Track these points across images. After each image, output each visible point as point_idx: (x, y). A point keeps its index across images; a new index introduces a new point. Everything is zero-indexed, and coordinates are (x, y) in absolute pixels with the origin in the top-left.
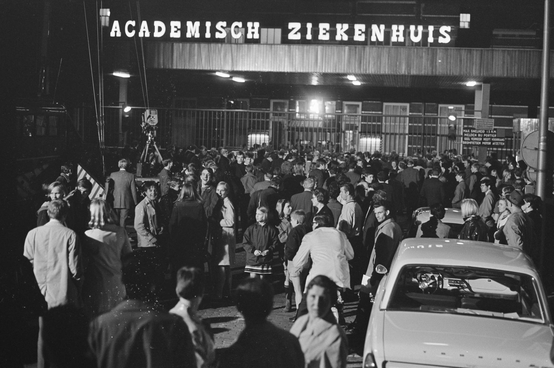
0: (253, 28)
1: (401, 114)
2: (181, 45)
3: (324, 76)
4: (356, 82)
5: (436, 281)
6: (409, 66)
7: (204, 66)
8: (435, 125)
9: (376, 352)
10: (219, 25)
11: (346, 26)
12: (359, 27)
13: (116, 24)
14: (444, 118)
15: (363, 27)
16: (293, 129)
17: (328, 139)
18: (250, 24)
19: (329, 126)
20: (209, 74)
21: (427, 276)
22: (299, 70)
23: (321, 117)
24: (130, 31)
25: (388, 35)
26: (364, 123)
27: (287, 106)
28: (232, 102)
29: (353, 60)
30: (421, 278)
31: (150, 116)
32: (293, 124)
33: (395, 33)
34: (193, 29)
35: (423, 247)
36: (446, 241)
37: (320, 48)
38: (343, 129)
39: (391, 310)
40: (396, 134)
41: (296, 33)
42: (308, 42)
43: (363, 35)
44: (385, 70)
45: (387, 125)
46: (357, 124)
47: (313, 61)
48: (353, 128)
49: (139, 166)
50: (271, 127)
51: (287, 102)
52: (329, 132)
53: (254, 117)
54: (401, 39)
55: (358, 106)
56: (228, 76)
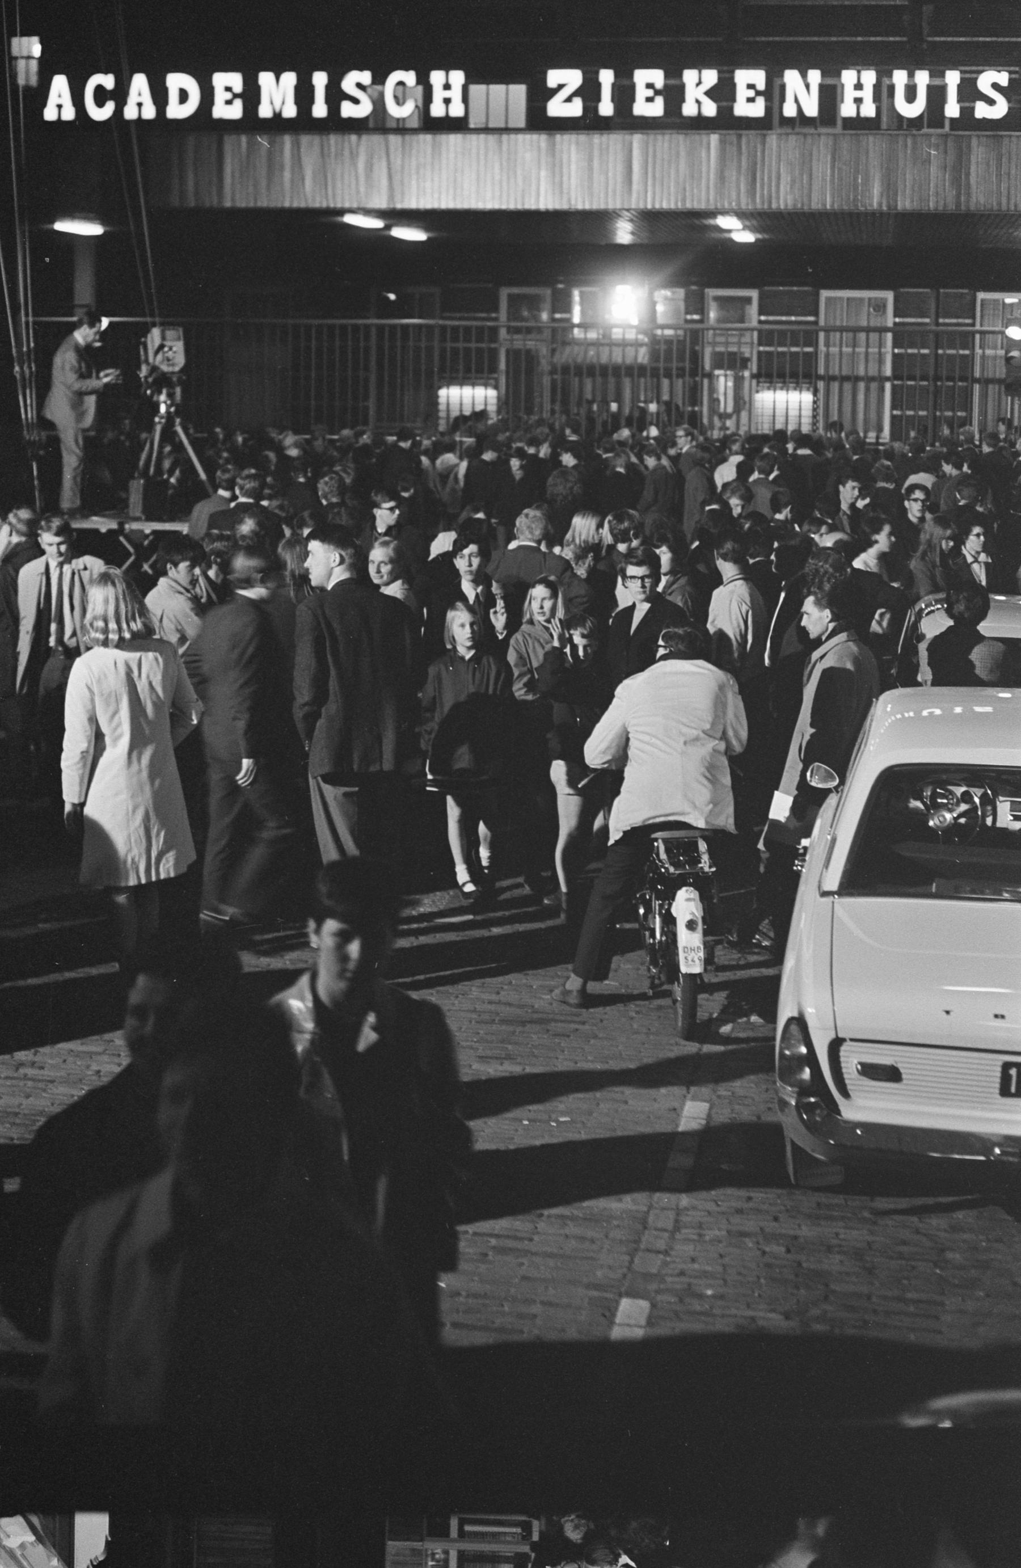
0: (447, 87)
1: (872, 324)
2: (244, 139)
3: (649, 218)
4: (744, 236)
5: (975, 808)
6: (890, 188)
7: (310, 195)
8: (967, 352)
9: (810, 1013)
10: (350, 82)
11: (711, 77)
12: (749, 78)
13: (60, 84)
14: (993, 332)
15: (758, 77)
16: (566, 369)
17: (666, 397)
18: (437, 77)
19: (668, 358)
20: (324, 220)
21: (951, 793)
22: (580, 202)
23: (645, 333)
24: (100, 103)
25: (830, 96)
26: (768, 349)
27: (547, 305)
28: (392, 297)
29: (732, 174)
30: (934, 796)
31: (161, 347)
32: (564, 356)
33: (850, 94)
34: (278, 93)
35: (938, 712)
36: (1001, 695)
37: (637, 139)
38: (707, 367)
39: (851, 895)
40: (857, 379)
41: (569, 100)
42: (603, 125)
43: (761, 102)
44: (824, 198)
45: (830, 352)
46: (746, 351)
47: (619, 179)
48: (734, 362)
49: (136, 489)
50: (502, 366)
51: (548, 292)
52: (668, 375)
53: (455, 339)
54: (869, 110)
55: (748, 300)
56: (377, 224)
